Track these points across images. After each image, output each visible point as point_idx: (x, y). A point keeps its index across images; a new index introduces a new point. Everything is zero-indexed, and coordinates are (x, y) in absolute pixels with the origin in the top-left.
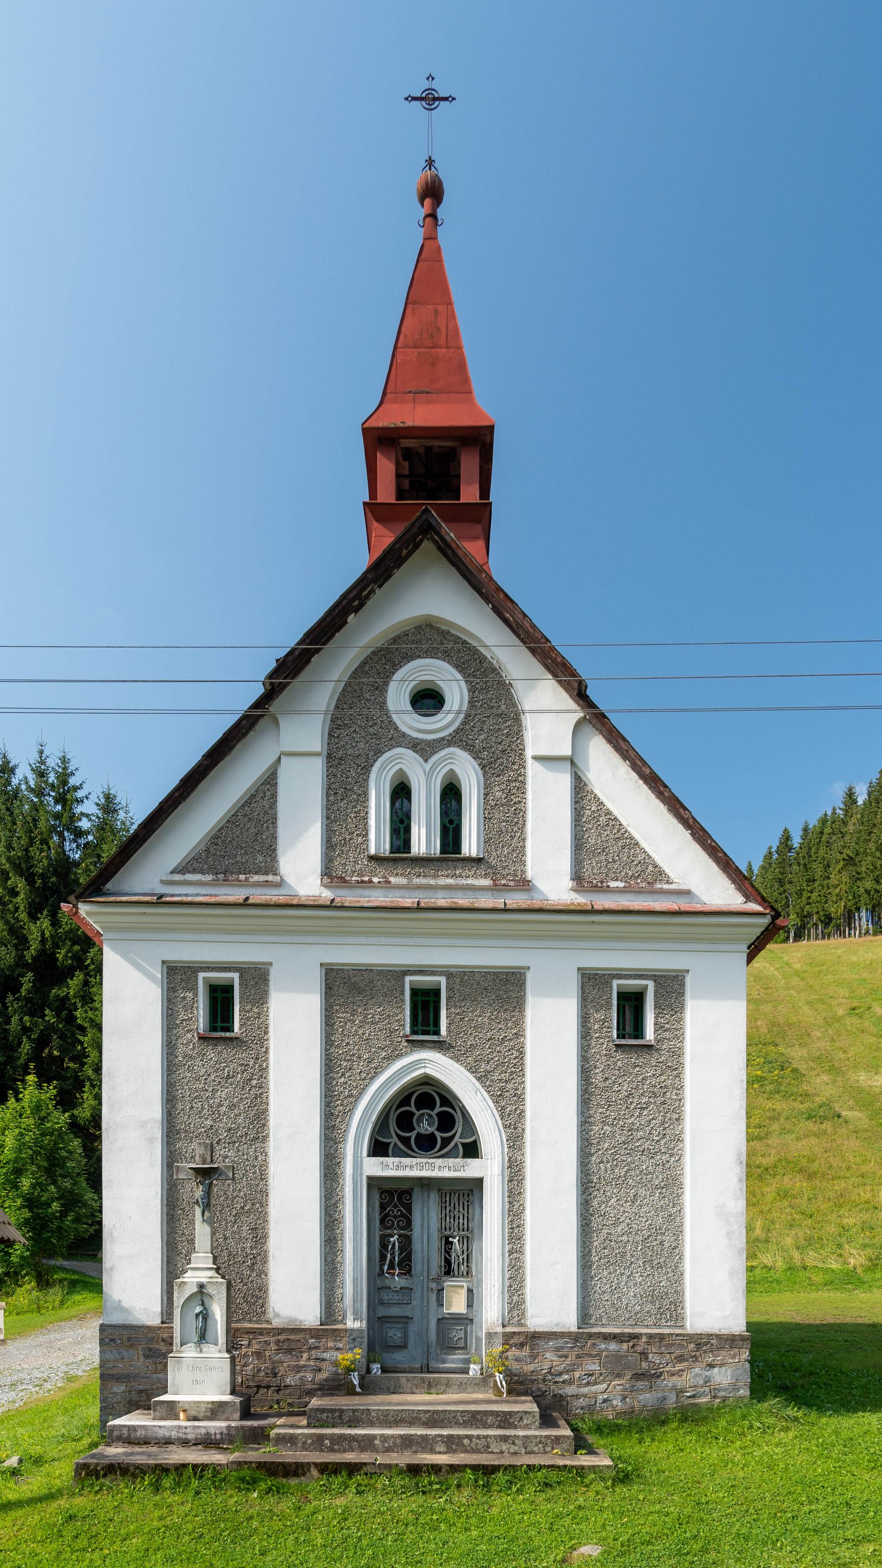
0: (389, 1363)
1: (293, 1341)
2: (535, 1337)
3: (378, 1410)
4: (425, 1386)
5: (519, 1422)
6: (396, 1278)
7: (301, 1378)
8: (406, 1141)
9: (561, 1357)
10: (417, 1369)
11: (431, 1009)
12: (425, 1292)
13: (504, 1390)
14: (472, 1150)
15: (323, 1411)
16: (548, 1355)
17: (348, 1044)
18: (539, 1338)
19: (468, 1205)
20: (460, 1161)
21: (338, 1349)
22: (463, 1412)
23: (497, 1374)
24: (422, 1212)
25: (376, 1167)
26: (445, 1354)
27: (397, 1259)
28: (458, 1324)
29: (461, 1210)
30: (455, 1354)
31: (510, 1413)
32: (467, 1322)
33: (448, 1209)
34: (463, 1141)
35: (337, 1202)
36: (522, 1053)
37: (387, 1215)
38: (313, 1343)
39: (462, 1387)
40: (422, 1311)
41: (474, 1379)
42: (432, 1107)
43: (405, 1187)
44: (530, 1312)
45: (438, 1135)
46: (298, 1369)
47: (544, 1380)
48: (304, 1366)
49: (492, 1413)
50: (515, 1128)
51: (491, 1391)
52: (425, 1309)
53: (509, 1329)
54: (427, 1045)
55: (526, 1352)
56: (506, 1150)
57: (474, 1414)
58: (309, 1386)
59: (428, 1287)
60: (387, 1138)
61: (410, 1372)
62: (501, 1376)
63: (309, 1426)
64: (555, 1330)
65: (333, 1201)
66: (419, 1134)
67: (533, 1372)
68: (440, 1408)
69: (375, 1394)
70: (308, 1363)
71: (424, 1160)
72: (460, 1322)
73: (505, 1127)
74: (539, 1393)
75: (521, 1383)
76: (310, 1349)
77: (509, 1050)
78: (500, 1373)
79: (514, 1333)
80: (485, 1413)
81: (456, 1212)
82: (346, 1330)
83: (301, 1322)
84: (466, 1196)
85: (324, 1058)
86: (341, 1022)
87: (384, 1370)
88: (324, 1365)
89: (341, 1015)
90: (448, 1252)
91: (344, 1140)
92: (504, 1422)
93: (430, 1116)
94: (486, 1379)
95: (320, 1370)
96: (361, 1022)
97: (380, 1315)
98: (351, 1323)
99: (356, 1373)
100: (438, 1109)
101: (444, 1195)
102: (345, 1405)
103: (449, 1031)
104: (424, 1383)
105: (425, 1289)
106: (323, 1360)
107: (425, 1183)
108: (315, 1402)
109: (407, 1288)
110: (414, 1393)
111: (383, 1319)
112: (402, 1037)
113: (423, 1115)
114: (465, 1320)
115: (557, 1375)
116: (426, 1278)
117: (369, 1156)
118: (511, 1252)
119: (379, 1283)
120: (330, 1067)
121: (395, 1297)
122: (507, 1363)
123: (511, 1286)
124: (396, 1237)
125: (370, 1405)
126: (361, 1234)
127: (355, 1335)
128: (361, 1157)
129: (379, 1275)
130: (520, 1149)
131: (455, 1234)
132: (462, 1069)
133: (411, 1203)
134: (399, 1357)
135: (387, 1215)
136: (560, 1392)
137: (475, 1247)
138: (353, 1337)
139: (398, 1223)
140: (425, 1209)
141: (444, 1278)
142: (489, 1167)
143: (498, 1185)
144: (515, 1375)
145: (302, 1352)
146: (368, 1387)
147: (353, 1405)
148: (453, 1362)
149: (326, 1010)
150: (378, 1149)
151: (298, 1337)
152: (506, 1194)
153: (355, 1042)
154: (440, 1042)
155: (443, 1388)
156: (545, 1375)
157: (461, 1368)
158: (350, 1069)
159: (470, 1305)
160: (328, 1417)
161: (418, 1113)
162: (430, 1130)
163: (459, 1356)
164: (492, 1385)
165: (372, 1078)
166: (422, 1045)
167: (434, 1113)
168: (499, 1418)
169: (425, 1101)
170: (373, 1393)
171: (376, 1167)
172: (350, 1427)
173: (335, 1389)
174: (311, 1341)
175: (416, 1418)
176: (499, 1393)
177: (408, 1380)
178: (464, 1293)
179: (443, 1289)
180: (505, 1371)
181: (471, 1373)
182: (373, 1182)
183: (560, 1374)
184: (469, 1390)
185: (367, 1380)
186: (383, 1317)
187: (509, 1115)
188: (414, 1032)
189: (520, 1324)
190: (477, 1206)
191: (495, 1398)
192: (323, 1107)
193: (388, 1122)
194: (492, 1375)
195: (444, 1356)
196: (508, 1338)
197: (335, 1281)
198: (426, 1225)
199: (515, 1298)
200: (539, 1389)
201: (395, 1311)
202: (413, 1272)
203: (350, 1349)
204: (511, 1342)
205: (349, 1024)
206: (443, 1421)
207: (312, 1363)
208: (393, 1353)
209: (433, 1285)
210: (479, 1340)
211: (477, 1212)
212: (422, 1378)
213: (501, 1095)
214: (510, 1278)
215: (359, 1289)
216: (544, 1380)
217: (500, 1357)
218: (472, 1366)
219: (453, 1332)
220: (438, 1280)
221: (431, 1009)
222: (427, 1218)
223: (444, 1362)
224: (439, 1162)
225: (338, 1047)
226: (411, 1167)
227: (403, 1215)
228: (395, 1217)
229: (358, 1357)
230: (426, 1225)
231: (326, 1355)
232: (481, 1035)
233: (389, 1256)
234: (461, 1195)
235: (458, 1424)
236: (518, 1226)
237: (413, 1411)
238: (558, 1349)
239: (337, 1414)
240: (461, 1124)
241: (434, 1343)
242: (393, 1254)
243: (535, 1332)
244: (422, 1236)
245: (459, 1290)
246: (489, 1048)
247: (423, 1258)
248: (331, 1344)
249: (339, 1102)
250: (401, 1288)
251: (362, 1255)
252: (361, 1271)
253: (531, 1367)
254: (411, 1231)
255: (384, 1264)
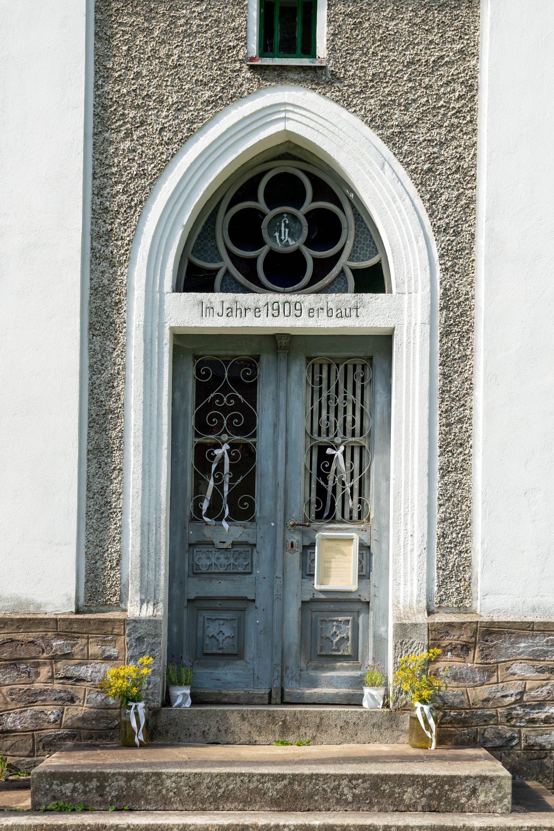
0: (208, 687)
1: (22, 643)
2: (492, 634)
3: (180, 776)
4: (277, 728)
5: (469, 798)
6: (225, 524)
7: (35, 717)
8: (247, 267)
9: (542, 671)
10: (262, 698)
11: (299, 19)
12: (280, 550)
13: (432, 736)
14: (372, 280)
15: (64, 777)
16: (516, 668)
17: (138, 75)
18: (499, 633)
19: (362, 387)
20: (349, 298)
21: (108, 658)
22: (352, 778)
23: (418, 705)
24: (276, 399)
25: (192, 312)
26: (316, 668)
27: (226, 488)
28: (341, 612)
29: (350, 396)
30: (334, 669)
31: (452, 781)
32: (358, 607)
33: (325, 394)
34: (355, 264)
35: (113, 377)
36: (472, 86)
37: (210, 406)
38: (61, 647)
39: (349, 730)
40: (272, 587)
41: (372, 714)
42: (299, 203)
43: (245, 353)
44: (481, 585)
45: (309, 254)
46: (31, 698)
47: (509, 717)
48: (42, 692)
49: (413, 780)
50: (456, 234)
51: (405, 738)
52: (279, 582)
53: (441, 618)
54: (291, 75)
55: (474, 660)
56: (439, 275)
57: (377, 781)
58: (52, 732)
59: (285, 541)
60: (212, 261)
61: (249, 703)
62: (426, 708)
63: (35, 809)
64: (530, 619)
65: (106, 376)
66: (272, 253)
67: (487, 700)
68: (306, 770)
69: (177, 746)
70: (49, 686)
71: (280, 298)
72: (345, 607)
73: (438, 230)
74: (498, 743)
75: (464, 722)
76: (55, 658)
77: (448, 83)
78: (423, 702)
79: (451, 625)
80: (400, 780)
81: (340, 399)
82: (125, 622)
83: (39, 606)
84: (359, 369)
85: (91, 102)
86: (125, 32)
87: (197, 699)
88: (80, 690)
89: (126, 19)
90: (323, 475)
91: (128, 259)
92: (439, 798)
93: (294, 218)
94: (394, 714)
95: (72, 700)
96: (164, 32)
97: (192, 596)
98: (136, 609)
99: (141, 705)
100: (309, 205)
101: (317, 368)
102: (111, 766)
103: (332, 49)
104: (274, 723)
105: (280, 545)
106: (79, 680)
107: (282, 345)
108: (53, 761)
109: (246, 544)
110: (255, 743)
111: (198, 603)
112: (241, 61)
113: (280, 216)
114: (354, 605)
115: (533, 707)
116: (280, 524)
117: (177, 289)
118: (445, 471)
119: (192, 535)
120: (102, 118)
121: (222, 561)
122: (436, 683)
123: (444, 536)
124: (226, 447)
125: (165, 764)
126: (159, 438)
127: (141, 632)
128: (161, 292)
129: (193, 520)
130: (465, 273)
131: (338, 440)
132: (356, 121)
133: (255, 384)
134: (228, 675)
135: (210, 406)
136: (540, 740)
137: (375, 467)
138: (141, 635)
139: (231, 419)
140: (282, 394)
141: (316, 525)
142: (403, 311)
143: (422, 344)
144: (452, 707)
145: (37, 665)
146: (159, 733)
147: (128, 766)
148: (330, 683)
149: (97, 9)
150: (194, 278)
151: (31, 636)
152: (438, 360)
153: (151, 72)
154: (315, 67)
155: (310, 733)
156: (510, 707)
157: (347, 695)
158: (142, 123)
159: (364, 575)
160: (74, 790)
161: (271, 214)
162: (293, 244)
163: (343, 672)
164: (407, 725)
165: (184, 141)
166: (280, 74)
167: (300, 213)
168: (428, 791)
169: (285, 190)
170: (176, 741)
171: (192, 312)
172: (119, 810)
173: (100, 737)
174: (57, 643)
175: (257, 790)
176: (421, 741)
177: (243, 718)
178: (352, 552)
179: (313, 545)
180: (432, 699)
181: (365, 704)
182: (185, 344)
183: (541, 705)
184: (361, 736)
185: (163, 718)
186: (197, 599)
187: (446, 207)
188: (266, 48)
189: (461, 608)
190: (379, 388)
191: (414, 752)
192: (90, 197)
193: (214, 230)
194: (407, 708)
195: (312, 673)
196: (437, 634)
197: (107, 528)
198: (282, 423)
199: (452, 558)
200: (499, 736)
201: (222, 588)
202: (257, 513)
203: (132, 657)
204: (445, 643)
205: (140, 36)
206: (311, 797)
207: (57, 686)
208: (216, 667)
209: (296, 538)
210: (380, 641)
211: (380, 398)
212: (270, 714)
213: (430, 170)
214: (443, 521)
215: (153, 542)
216: (509, 717)
217: (424, 671)
218: (367, 691)
219: (329, 627)
220: (303, 526)
221: (299, 19)
222: (285, 415)
223: (314, 683)
224: (309, 300)
225: (119, 80)
226: (257, 310)
227: (239, 406)
228: (225, 410)
229: (145, 671)
230: (282, 423)
231: (85, 671)
232: (393, 56)
233: (211, 483)
234: (350, 368)
235: (343, 804)
236: (460, 421)
237: (251, 776)
238: (535, 657)
239: (94, 783)
240: (352, 233)
241: (295, 648)
242: (219, 480)
243: (492, 623)
244: (275, 445)
245: (344, 547)
246: (410, 80)
247: (277, 485)
248: (94, 649)
249: (120, 187)
250: (234, 544)
251: (158, 479)
252: (158, 510)
253: (483, 692)
254: (254, 435)
255: (201, 500)
